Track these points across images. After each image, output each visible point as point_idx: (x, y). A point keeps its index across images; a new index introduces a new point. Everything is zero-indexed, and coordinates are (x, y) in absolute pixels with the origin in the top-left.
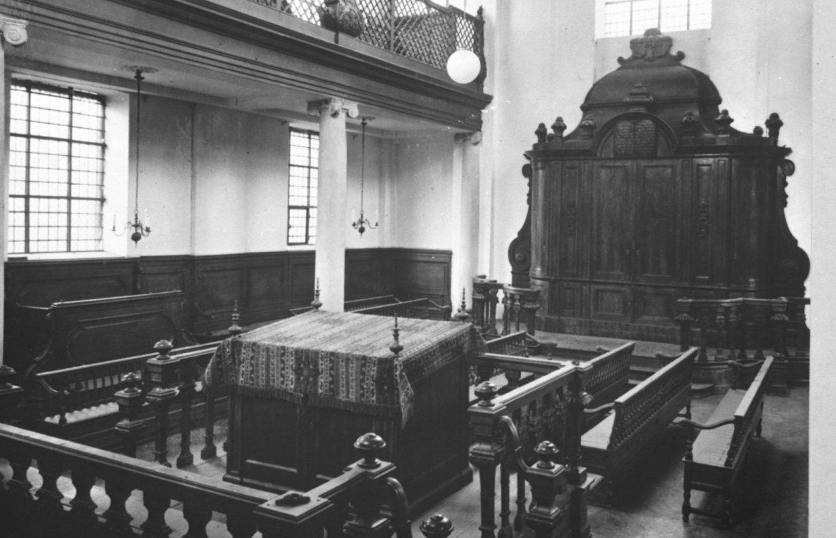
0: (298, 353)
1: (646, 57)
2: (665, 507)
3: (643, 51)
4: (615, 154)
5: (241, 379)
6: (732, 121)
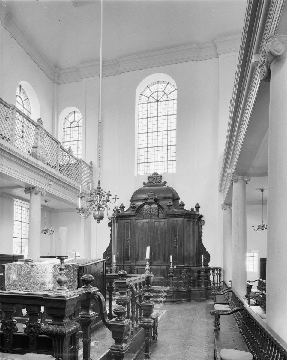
1: (153, 182)
3: (151, 180)
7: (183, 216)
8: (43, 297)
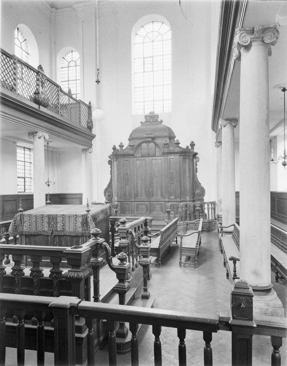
0: (49, 216)
2: (175, 262)
4: (142, 155)
5: (25, 228)
6: (179, 143)
7: (178, 154)
8: (63, 251)
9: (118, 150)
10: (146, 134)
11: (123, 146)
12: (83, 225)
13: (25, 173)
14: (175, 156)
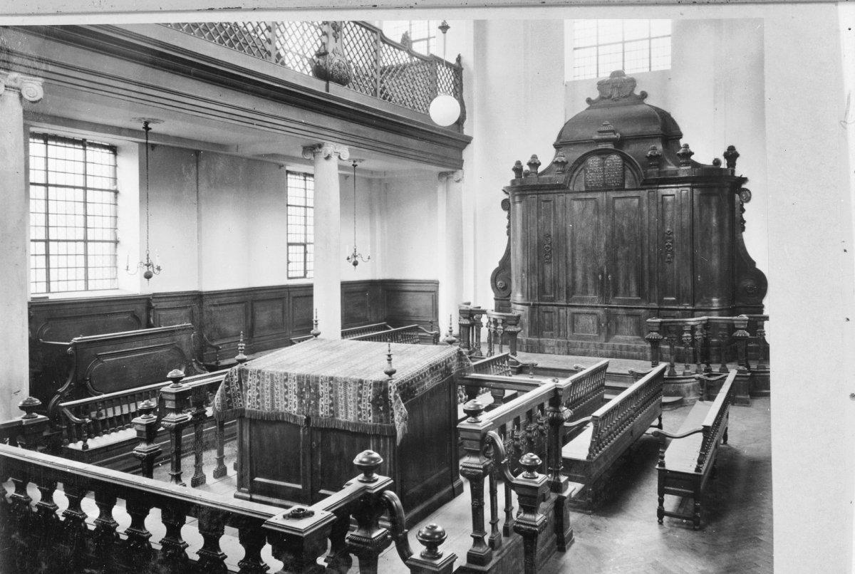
4: (586, 187)
5: (248, 404)
6: (692, 154)
9: (527, 174)
10: (600, 132)
11: (540, 164)
12: (376, 411)
13: (306, 234)
14: (678, 187)
